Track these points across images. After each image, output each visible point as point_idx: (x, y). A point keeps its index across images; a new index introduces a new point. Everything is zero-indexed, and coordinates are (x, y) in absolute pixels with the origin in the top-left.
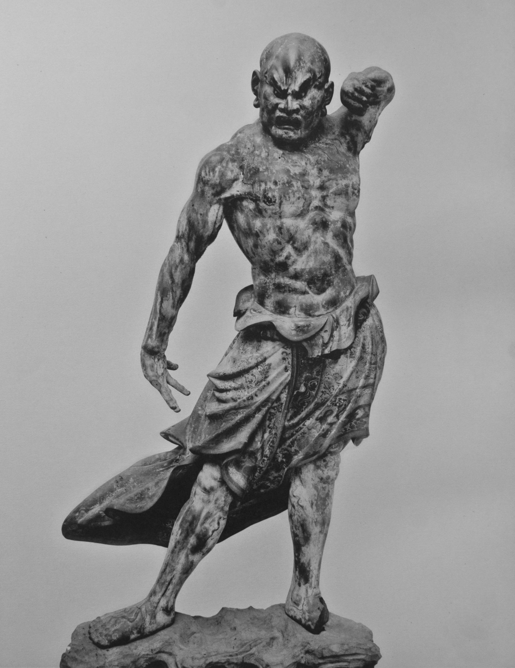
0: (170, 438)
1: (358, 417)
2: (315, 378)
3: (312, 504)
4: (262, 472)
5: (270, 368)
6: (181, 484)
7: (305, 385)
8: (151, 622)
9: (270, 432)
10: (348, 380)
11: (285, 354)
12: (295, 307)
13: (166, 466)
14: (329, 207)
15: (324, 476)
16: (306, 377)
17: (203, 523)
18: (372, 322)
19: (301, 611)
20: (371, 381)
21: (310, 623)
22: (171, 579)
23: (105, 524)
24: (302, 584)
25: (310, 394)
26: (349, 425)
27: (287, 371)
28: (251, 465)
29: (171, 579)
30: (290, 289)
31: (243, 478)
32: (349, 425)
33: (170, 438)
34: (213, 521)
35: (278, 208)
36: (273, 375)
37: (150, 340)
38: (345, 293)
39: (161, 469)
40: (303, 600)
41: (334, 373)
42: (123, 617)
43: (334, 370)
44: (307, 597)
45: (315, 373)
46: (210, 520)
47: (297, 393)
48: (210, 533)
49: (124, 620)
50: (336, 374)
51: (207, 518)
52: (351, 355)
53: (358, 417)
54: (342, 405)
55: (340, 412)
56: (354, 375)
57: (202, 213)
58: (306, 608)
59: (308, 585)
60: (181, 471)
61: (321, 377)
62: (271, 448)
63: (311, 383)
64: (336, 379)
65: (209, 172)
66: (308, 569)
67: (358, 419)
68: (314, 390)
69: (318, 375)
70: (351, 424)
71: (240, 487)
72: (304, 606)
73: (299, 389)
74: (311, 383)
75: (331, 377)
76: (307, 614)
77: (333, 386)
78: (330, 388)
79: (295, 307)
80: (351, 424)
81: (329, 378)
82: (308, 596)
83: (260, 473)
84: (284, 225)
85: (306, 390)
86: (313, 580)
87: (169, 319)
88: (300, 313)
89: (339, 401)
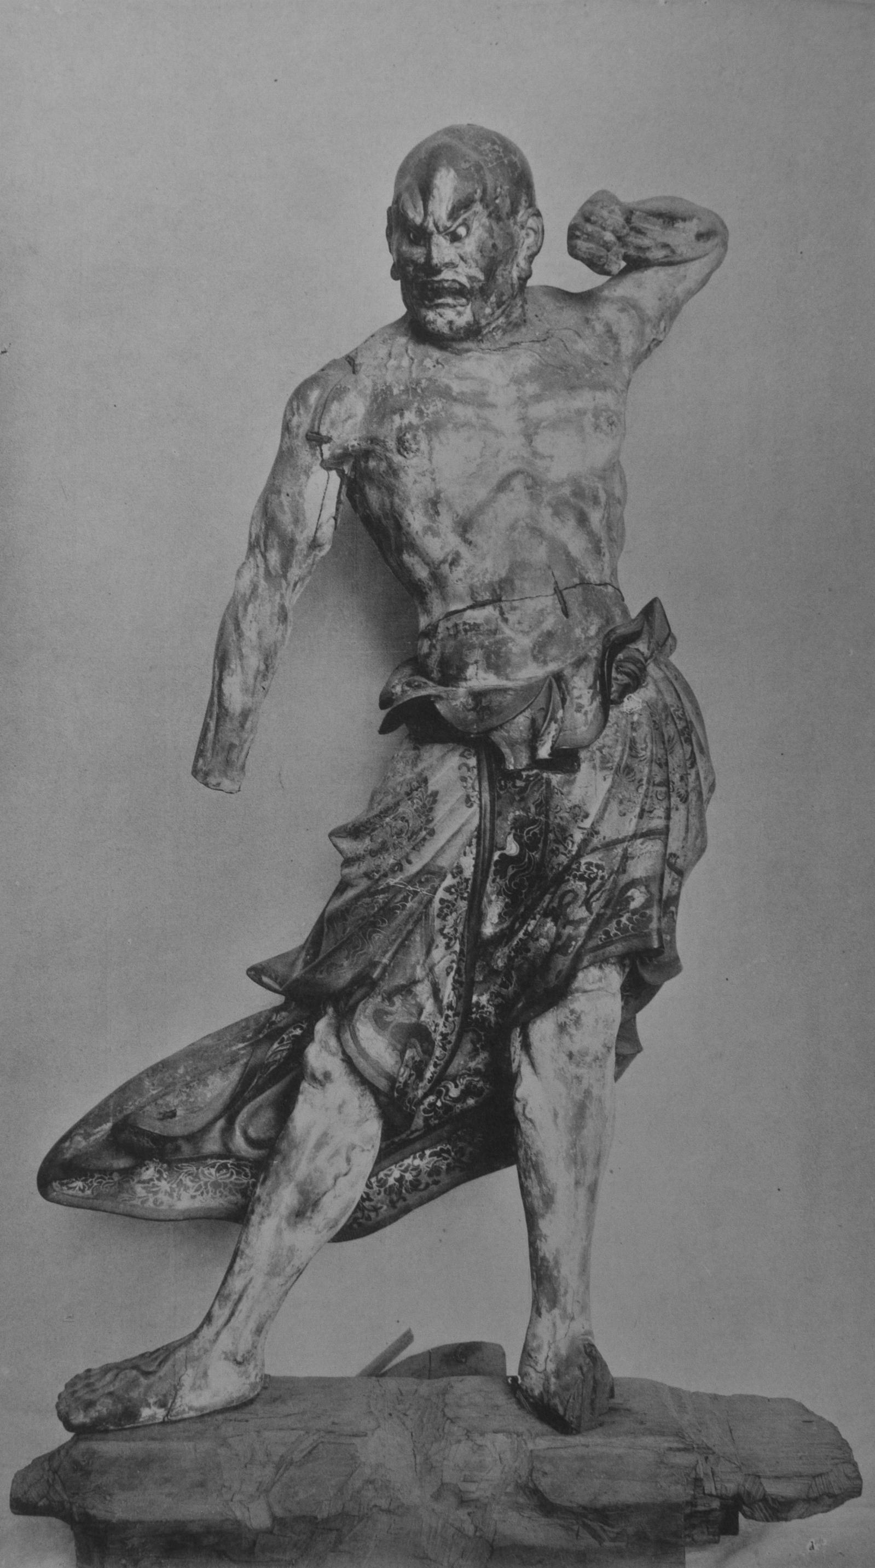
0: (265, 979)
1: (633, 905)
2: (534, 822)
3: (556, 1115)
4: (448, 1047)
5: (435, 802)
6: (272, 1072)
7: (518, 839)
8: (194, 1384)
9: (448, 947)
10: (600, 817)
11: (464, 769)
12: (476, 662)
13: (251, 1038)
14: (543, 457)
15: (575, 1048)
16: (516, 820)
17: (312, 1159)
18: (654, 695)
19: (542, 1375)
20: (657, 823)
21: (557, 1401)
22: (245, 1288)
23: (107, 1157)
24: (543, 1311)
25: (529, 858)
26: (614, 922)
27: (472, 805)
28: (407, 1022)
29: (245, 1288)
30: (467, 627)
31: (390, 1050)
32: (614, 922)
33: (265, 979)
34: (337, 1153)
35: (426, 461)
36: (440, 811)
37: (201, 761)
38: (585, 630)
39: (241, 1045)
40: (545, 1347)
41: (570, 805)
42: (135, 1367)
43: (570, 797)
44: (554, 1342)
45: (533, 809)
46: (326, 1152)
47: (501, 856)
48: (330, 1181)
49: (134, 1372)
50: (575, 806)
51: (319, 1146)
52: (602, 762)
53: (633, 905)
54: (595, 878)
55: (592, 895)
56: (614, 806)
57: (290, 491)
58: (551, 1367)
59: (556, 1312)
60: (276, 1045)
61: (547, 817)
62: (458, 985)
63: (528, 833)
64: (575, 818)
65: (298, 409)
66: (555, 1273)
67: (634, 912)
68: (536, 848)
69: (539, 814)
70: (619, 923)
71: (387, 1073)
72: (545, 1361)
73: (503, 849)
74: (528, 833)
75: (566, 815)
76: (553, 1380)
77: (571, 836)
78: (565, 839)
79: (476, 662)
80: (619, 923)
81: (561, 818)
82: (558, 1338)
83: (444, 1048)
84: (442, 495)
85: (521, 850)
86: (568, 1301)
87: (237, 714)
88: (485, 676)
89: (588, 868)
